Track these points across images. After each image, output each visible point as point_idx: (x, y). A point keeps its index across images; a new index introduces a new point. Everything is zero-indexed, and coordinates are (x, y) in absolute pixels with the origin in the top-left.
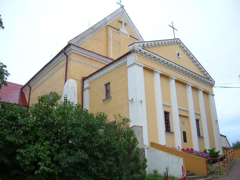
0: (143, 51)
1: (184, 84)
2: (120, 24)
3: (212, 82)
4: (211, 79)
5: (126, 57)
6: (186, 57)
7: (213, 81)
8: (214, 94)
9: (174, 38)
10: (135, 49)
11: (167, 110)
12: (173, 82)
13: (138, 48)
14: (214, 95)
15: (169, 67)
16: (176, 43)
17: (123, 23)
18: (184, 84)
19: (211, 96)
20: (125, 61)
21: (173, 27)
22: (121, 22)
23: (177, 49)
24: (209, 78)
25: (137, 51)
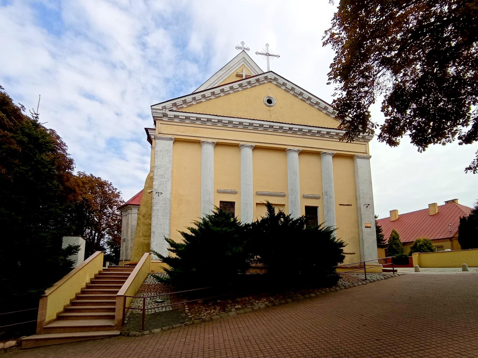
0: (171, 114)
14: (369, 157)
25: (161, 117)
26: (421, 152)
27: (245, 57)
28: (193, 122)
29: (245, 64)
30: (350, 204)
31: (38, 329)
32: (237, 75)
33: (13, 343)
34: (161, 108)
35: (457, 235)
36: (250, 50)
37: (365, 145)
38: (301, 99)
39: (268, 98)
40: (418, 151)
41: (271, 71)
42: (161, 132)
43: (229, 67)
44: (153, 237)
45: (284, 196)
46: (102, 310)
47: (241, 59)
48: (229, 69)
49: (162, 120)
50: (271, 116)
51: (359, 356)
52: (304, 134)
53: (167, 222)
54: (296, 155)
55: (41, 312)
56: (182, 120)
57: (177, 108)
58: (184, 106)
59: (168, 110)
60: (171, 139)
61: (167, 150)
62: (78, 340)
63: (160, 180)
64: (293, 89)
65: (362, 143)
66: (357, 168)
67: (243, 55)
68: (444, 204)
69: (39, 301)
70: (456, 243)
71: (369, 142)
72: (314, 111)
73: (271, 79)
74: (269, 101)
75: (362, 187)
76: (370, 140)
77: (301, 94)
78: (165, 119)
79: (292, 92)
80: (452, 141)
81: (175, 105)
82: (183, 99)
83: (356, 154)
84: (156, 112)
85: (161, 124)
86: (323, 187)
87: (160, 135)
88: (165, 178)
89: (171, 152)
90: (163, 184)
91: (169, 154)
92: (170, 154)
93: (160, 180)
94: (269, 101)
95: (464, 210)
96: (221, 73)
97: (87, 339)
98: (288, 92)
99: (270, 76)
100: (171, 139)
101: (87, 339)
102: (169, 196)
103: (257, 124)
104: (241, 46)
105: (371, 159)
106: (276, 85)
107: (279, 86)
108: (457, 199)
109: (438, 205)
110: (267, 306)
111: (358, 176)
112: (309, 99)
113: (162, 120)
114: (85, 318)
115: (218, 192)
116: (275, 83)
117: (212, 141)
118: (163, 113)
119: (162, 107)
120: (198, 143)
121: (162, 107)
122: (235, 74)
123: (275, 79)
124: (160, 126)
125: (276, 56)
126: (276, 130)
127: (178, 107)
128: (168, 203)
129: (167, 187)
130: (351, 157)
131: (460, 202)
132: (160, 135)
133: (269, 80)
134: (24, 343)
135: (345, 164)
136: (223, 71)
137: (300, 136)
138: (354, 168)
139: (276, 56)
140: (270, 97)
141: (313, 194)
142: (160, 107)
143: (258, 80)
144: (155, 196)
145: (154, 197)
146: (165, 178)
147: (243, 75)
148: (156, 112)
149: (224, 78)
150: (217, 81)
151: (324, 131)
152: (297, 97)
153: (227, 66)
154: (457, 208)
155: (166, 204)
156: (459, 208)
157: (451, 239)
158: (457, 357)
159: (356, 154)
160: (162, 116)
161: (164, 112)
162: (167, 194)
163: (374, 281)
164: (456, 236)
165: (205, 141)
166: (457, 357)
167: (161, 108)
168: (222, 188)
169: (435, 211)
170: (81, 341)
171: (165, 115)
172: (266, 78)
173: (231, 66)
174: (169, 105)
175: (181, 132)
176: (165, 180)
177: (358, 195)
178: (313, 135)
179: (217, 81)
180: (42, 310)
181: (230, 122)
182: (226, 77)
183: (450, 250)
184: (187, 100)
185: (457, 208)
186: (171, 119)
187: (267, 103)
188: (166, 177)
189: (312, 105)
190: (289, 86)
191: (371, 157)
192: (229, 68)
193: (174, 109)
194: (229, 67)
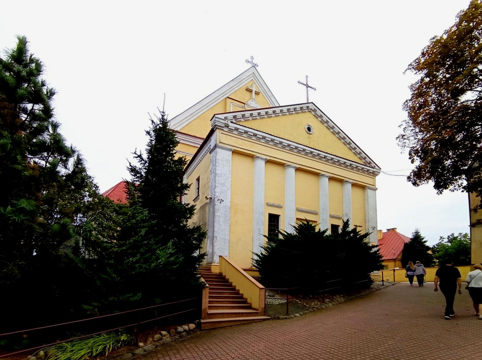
0: (232, 126)
1: (341, 181)
2: (248, 94)
3: (374, 170)
4: (373, 165)
5: (210, 139)
6: (328, 133)
7: (377, 167)
8: (377, 187)
9: (306, 102)
10: (216, 124)
11: (275, 211)
12: (261, 164)
13: (223, 123)
14: (375, 189)
15: (367, 166)
16: (300, 112)
17: (254, 92)
18: (341, 181)
19: (369, 192)
20: (209, 146)
21: (308, 86)
22: (250, 91)
23: (308, 119)
24: (370, 163)
25: (223, 127)
26: (439, 194)
27: (255, 73)
28: (250, 137)
29: (254, 80)
30: (361, 226)
31: (203, 315)
32: (256, 92)
33: (192, 326)
34: (223, 118)
35: (400, 257)
36: (259, 66)
37: (373, 179)
38: (332, 132)
39: (308, 126)
40: (437, 193)
41: (312, 103)
42: (222, 142)
43: (240, 79)
44: (215, 242)
45: (316, 214)
46: (228, 302)
47: (251, 74)
48: (240, 82)
49: (223, 130)
50: (310, 142)
51: (292, 358)
52: (334, 163)
53: (228, 228)
54: (327, 180)
55: (205, 300)
56: (240, 134)
57: (235, 120)
58: (242, 120)
59: (230, 121)
60: (230, 150)
61: (227, 160)
62: (242, 323)
63: (221, 188)
64: (327, 122)
65: (372, 177)
66: (368, 197)
67: (253, 70)
68: (386, 231)
69: (202, 291)
70: (399, 263)
71: (376, 177)
72: (340, 144)
73: (311, 109)
74: (309, 129)
75: (371, 213)
76: (377, 175)
77: (333, 128)
78: (225, 129)
79: (326, 125)
80: (458, 189)
81: (235, 117)
82: (243, 113)
83: (367, 185)
84: (219, 121)
85: (221, 133)
86: (344, 209)
87: (221, 145)
88: (225, 186)
89: (231, 162)
90: (224, 192)
91: (229, 164)
92: (230, 164)
93: (221, 188)
94: (309, 129)
95: (402, 237)
96: (233, 84)
97: (249, 322)
98: (323, 124)
99: (311, 106)
100: (230, 150)
101: (249, 322)
102: (229, 204)
103: (301, 148)
104: (250, 60)
105: (377, 191)
106: (314, 115)
107: (317, 116)
108: (396, 228)
109: (383, 232)
110: (345, 301)
111: (368, 203)
112: (338, 133)
113: (223, 130)
114: (222, 308)
115: (267, 205)
116: (313, 113)
117: (265, 158)
118: (225, 123)
119: (225, 117)
120: (252, 157)
121: (225, 117)
122: (245, 87)
123: (315, 111)
124: (220, 136)
125: (301, 83)
126: (314, 156)
127: (237, 120)
128: (228, 210)
129: (227, 196)
130: (363, 187)
131: (398, 231)
132: (221, 145)
133: (310, 110)
134: (203, 325)
135: (358, 191)
136: (234, 82)
137: (331, 164)
138: (365, 197)
139: (301, 83)
140: (310, 126)
141: (338, 214)
142: (222, 116)
143: (301, 108)
144: (217, 203)
145: (216, 203)
146: (225, 186)
147: (252, 90)
148: (219, 121)
149: (235, 90)
150: (228, 91)
151: (348, 163)
152: (329, 129)
153: (238, 78)
154: (397, 236)
155: (226, 211)
156: (399, 236)
157: (394, 260)
158: (353, 359)
159: (367, 185)
160: (224, 126)
161: (226, 122)
162: (227, 203)
163: (388, 286)
164: (398, 258)
165: (259, 156)
166: (353, 359)
167: (223, 118)
168: (271, 202)
169: (381, 237)
170: (245, 324)
171: (227, 126)
172: (308, 107)
173: (242, 79)
174: (230, 116)
175: (239, 144)
176: (226, 188)
177: (367, 219)
178: (340, 164)
179: (228, 91)
180: (205, 299)
181: (281, 143)
182: (237, 89)
183: (398, 268)
184: (246, 115)
185: (397, 236)
186: (231, 130)
187: (307, 130)
188: (226, 186)
189: (340, 138)
190: (325, 118)
191: (377, 189)
192: (240, 80)
193: (234, 121)
194: (240, 79)
